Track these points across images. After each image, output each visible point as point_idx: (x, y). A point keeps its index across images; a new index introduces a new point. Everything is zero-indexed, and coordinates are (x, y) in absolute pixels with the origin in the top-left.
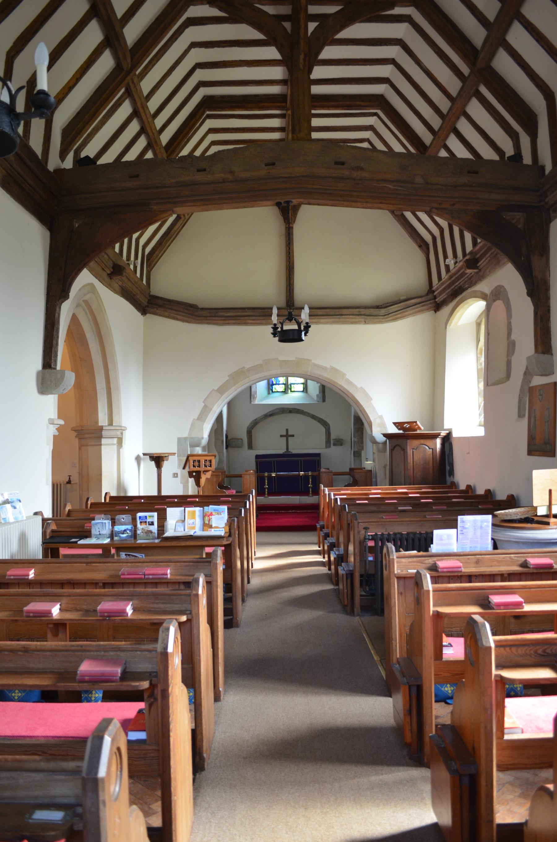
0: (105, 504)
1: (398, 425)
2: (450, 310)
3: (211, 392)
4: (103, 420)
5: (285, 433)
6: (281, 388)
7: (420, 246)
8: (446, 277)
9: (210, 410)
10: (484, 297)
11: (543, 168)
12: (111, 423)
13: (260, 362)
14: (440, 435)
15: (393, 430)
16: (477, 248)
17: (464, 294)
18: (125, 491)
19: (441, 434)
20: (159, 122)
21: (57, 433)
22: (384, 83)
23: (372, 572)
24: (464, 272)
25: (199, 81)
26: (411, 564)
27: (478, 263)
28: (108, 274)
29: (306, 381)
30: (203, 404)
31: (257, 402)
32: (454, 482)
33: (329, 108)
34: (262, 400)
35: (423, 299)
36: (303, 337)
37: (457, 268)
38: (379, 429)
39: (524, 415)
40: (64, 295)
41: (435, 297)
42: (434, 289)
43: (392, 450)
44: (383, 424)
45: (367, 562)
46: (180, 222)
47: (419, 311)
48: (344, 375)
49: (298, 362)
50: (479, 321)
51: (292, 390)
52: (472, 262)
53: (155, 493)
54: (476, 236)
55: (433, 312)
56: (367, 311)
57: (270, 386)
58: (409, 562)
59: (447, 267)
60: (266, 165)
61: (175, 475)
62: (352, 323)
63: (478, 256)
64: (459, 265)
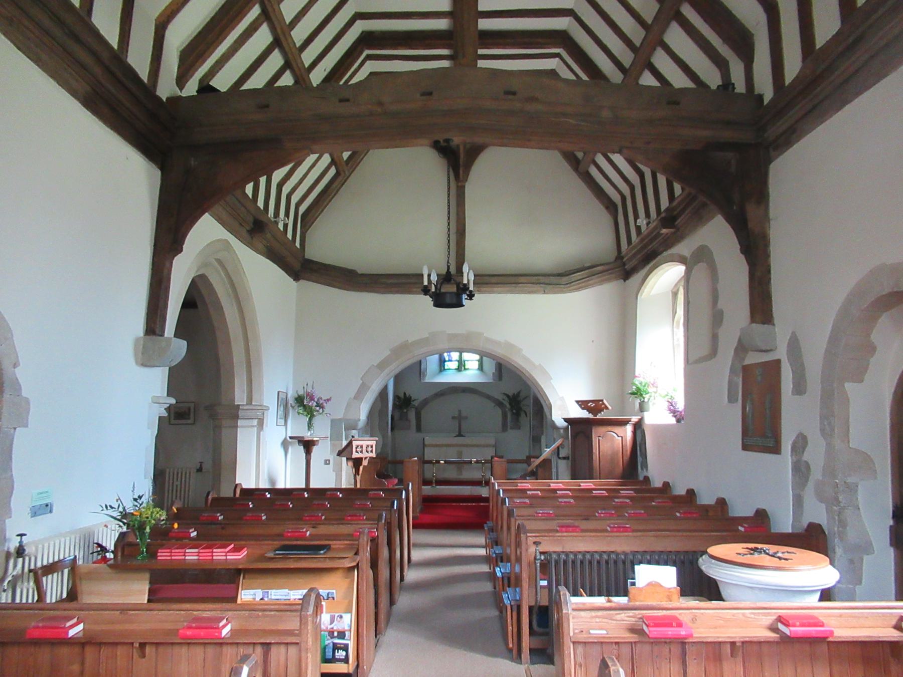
0: (234, 499)
1: (583, 404)
4: (240, 398)
5: (456, 415)
6: (453, 365)
7: (607, 208)
10: (682, 260)
11: (760, 97)
16: (675, 203)
17: (657, 259)
20: (308, 57)
22: (567, 16)
23: (544, 602)
25: (356, 13)
26: (594, 620)
28: (248, 231)
29: (481, 358)
31: (428, 379)
33: (504, 46)
36: (465, 302)
37: (650, 229)
39: (737, 400)
41: (624, 264)
43: (574, 437)
45: (539, 588)
46: (340, 179)
48: (520, 350)
49: (468, 337)
50: (675, 290)
52: (669, 219)
57: (442, 362)
58: (592, 617)
59: (638, 228)
60: (423, 94)
61: (327, 462)
62: (530, 292)
63: (675, 213)
64: (652, 226)
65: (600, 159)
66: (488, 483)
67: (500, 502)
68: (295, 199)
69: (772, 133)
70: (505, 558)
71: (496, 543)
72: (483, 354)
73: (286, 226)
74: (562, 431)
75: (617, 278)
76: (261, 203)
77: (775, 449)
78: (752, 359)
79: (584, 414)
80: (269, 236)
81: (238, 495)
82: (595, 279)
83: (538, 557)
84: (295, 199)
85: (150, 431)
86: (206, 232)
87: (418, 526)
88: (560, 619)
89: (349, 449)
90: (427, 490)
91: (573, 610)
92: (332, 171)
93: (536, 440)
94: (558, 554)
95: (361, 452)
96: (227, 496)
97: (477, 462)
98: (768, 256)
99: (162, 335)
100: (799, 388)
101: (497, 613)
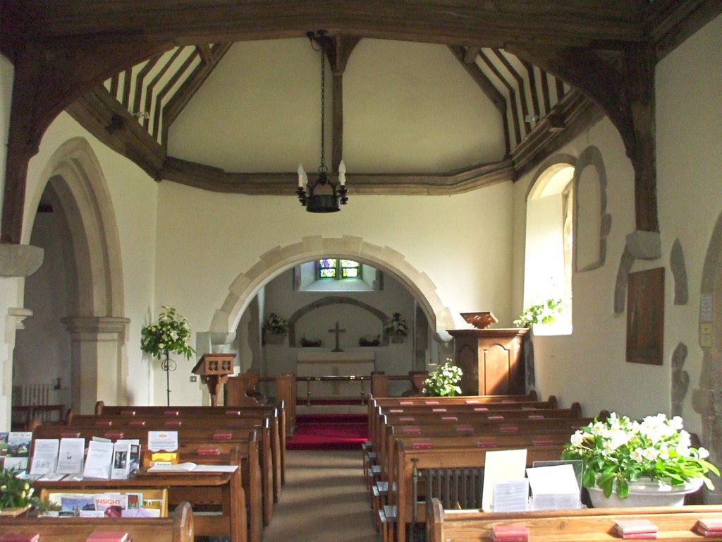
2: (532, 178)
3: (239, 277)
4: (98, 307)
5: (334, 328)
6: (329, 273)
7: (495, 102)
8: (526, 139)
9: (237, 298)
10: (571, 161)
12: (109, 315)
13: (299, 240)
14: (518, 333)
15: (463, 325)
17: (548, 158)
18: (129, 397)
19: (520, 332)
21: (22, 327)
23: (421, 519)
24: (547, 131)
26: (466, 529)
27: (564, 119)
28: (107, 128)
30: (229, 292)
32: (535, 392)
34: (308, 287)
35: (500, 165)
38: (444, 325)
39: (622, 310)
40: (32, 147)
41: (513, 164)
42: (512, 152)
44: (450, 319)
46: (206, 68)
47: (495, 180)
49: (346, 241)
51: (344, 275)
52: (558, 118)
53: (166, 405)
54: (561, 79)
55: (511, 181)
56: (431, 179)
57: (318, 269)
58: (463, 527)
59: (528, 125)
62: (412, 193)
64: (542, 123)
65: (489, 52)
66: (367, 401)
67: (384, 431)
68: (157, 90)
69: (657, 33)
70: (390, 499)
71: (374, 462)
72: (362, 262)
73: (146, 121)
74: (446, 344)
75: (505, 179)
76: (120, 98)
77: (657, 359)
78: (639, 266)
79: (470, 327)
80: (128, 132)
81: (99, 413)
82: (482, 180)
83: (416, 474)
84: (157, 90)
85: (7, 345)
86: (64, 129)
87: (292, 447)
88: (433, 529)
89: (202, 365)
90: (302, 410)
91: (445, 520)
92: (197, 60)
93: (420, 355)
94: (436, 470)
95: (216, 369)
96: (89, 414)
97: (357, 379)
98: (653, 160)
99: (18, 242)
100: (681, 299)
101: (374, 532)
